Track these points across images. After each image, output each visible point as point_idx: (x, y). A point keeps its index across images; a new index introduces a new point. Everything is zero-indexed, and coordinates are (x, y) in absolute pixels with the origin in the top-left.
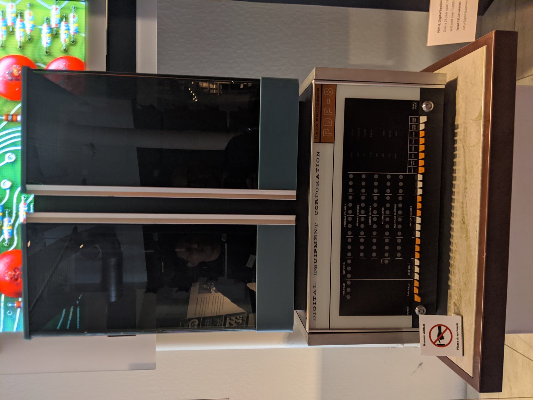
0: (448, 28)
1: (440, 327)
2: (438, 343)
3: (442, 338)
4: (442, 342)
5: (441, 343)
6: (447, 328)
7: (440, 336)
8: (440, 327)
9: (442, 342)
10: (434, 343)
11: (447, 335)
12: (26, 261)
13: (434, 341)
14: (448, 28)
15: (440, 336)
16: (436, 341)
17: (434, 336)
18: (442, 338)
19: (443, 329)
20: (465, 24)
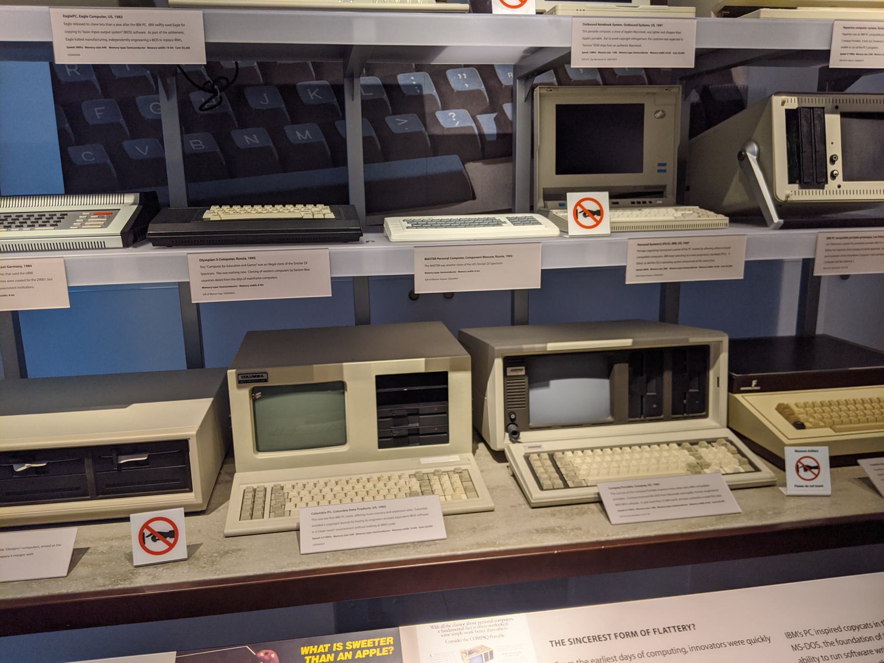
0: (70, 36)
1: (817, 467)
2: (800, 465)
3: (806, 470)
4: (801, 470)
5: (146, 539)
6: (817, 476)
7: (807, 468)
8: (817, 467)
9: (801, 470)
10: (799, 461)
11: (809, 475)
12: (688, 120)
13: (167, 547)
14: (70, 36)
15: (807, 468)
16: (168, 543)
17: (806, 462)
18: (806, 470)
19: (816, 471)
20: (641, 655)
